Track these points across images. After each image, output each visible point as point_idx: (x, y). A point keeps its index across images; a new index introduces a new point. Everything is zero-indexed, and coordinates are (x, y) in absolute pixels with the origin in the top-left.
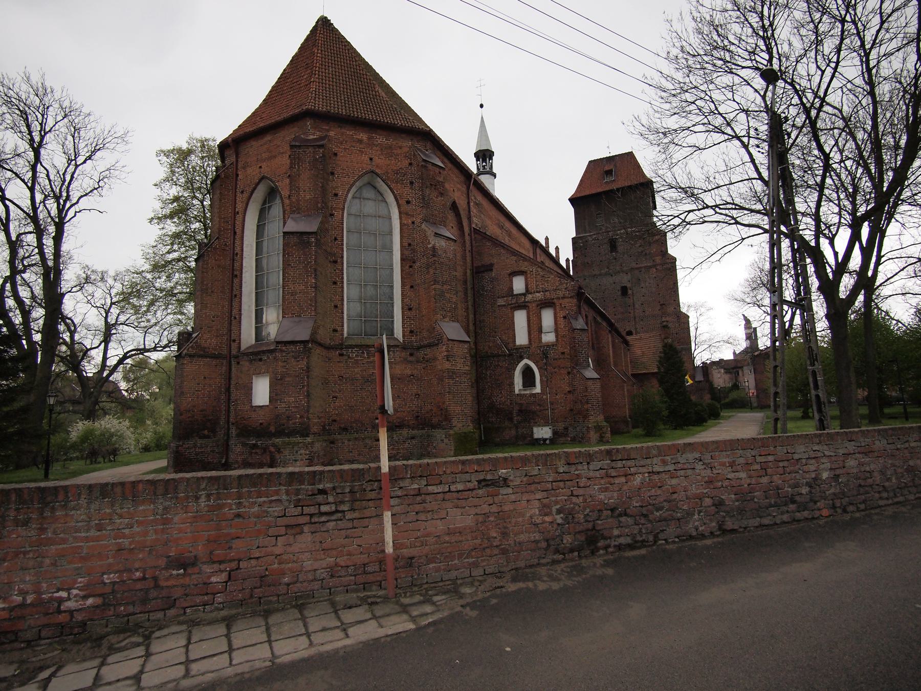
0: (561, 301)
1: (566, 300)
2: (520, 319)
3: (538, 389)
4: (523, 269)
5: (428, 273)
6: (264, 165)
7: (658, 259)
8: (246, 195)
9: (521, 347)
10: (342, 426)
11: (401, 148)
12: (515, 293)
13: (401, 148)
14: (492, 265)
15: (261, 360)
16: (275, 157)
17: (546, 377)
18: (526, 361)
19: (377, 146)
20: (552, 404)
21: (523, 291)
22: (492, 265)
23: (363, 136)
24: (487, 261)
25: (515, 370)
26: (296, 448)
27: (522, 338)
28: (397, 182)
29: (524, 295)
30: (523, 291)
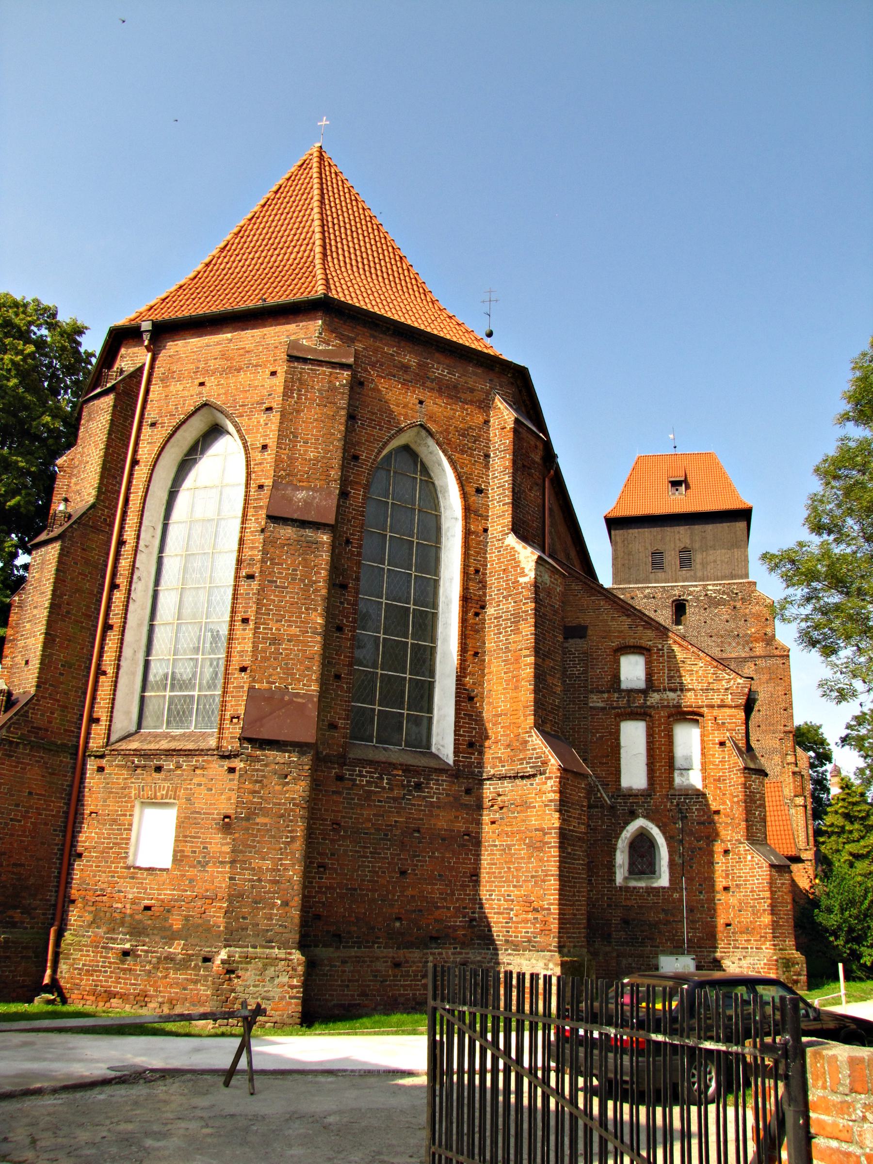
0: (716, 712)
1: (728, 711)
2: (633, 736)
3: (664, 880)
4: (644, 643)
5: (517, 631)
6: (211, 382)
7: (759, 648)
8: (160, 434)
9: (631, 794)
10: (333, 929)
11: (472, 391)
12: (623, 686)
13: (472, 391)
14: (585, 628)
15: (158, 769)
16: (239, 370)
17: (682, 855)
18: (640, 822)
19: (432, 381)
20: (691, 910)
21: (641, 684)
22: (585, 628)
23: (411, 359)
24: (585, 619)
25: (617, 837)
26: (271, 971)
27: (634, 775)
28: (463, 452)
29: (644, 692)
30: (641, 684)
